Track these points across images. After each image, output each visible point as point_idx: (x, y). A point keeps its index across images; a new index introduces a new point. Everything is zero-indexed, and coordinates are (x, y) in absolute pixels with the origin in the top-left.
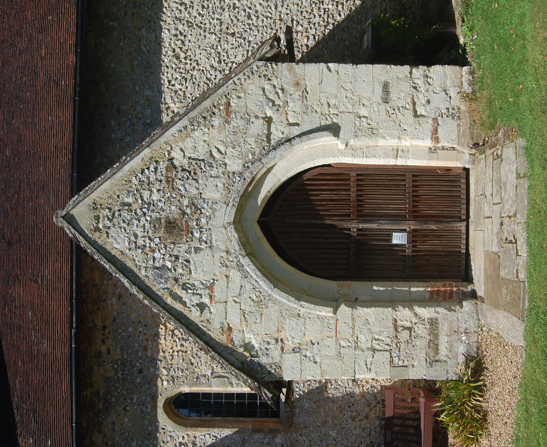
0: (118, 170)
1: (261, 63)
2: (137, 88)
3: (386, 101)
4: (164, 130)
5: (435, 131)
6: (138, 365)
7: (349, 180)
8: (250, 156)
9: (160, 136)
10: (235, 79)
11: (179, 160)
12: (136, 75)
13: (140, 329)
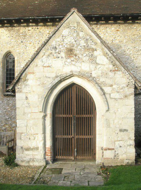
0: (92, 31)
1: (134, 83)
2: (126, 37)
3: (121, 130)
4: (107, 47)
5: (109, 149)
6: (24, 41)
7: (90, 114)
8: (98, 80)
9: (105, 46)
10: (127, 73)
11: (96, 53)
12: (131, 36)
13: (37, 41)
